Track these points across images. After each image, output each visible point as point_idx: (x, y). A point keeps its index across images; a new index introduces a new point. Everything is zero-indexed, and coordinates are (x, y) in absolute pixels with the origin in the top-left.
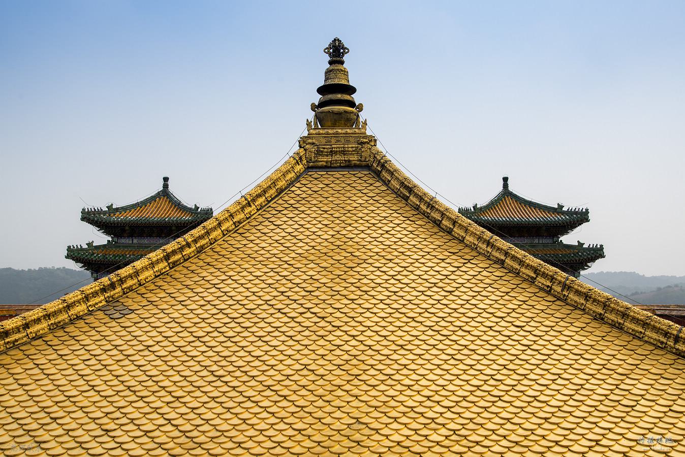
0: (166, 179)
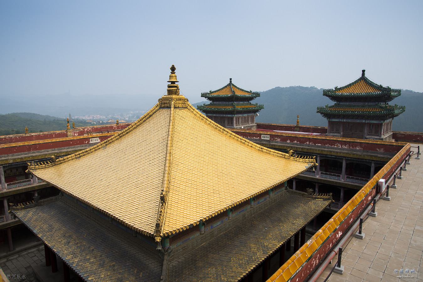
0: (231, 79)
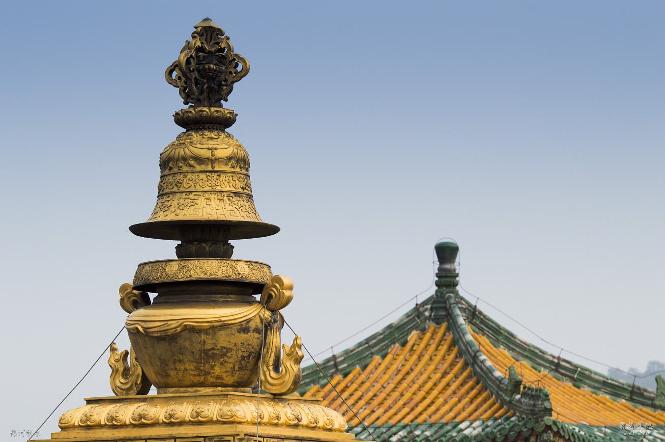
0: (446, 253)
